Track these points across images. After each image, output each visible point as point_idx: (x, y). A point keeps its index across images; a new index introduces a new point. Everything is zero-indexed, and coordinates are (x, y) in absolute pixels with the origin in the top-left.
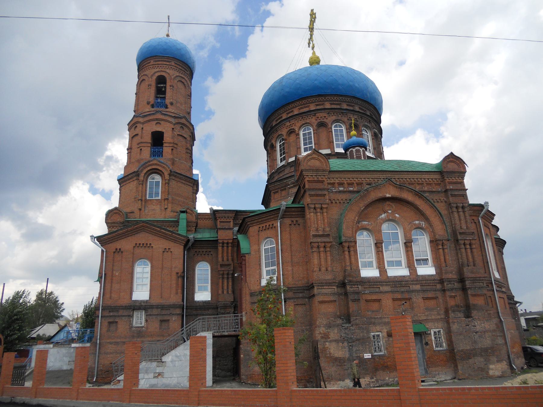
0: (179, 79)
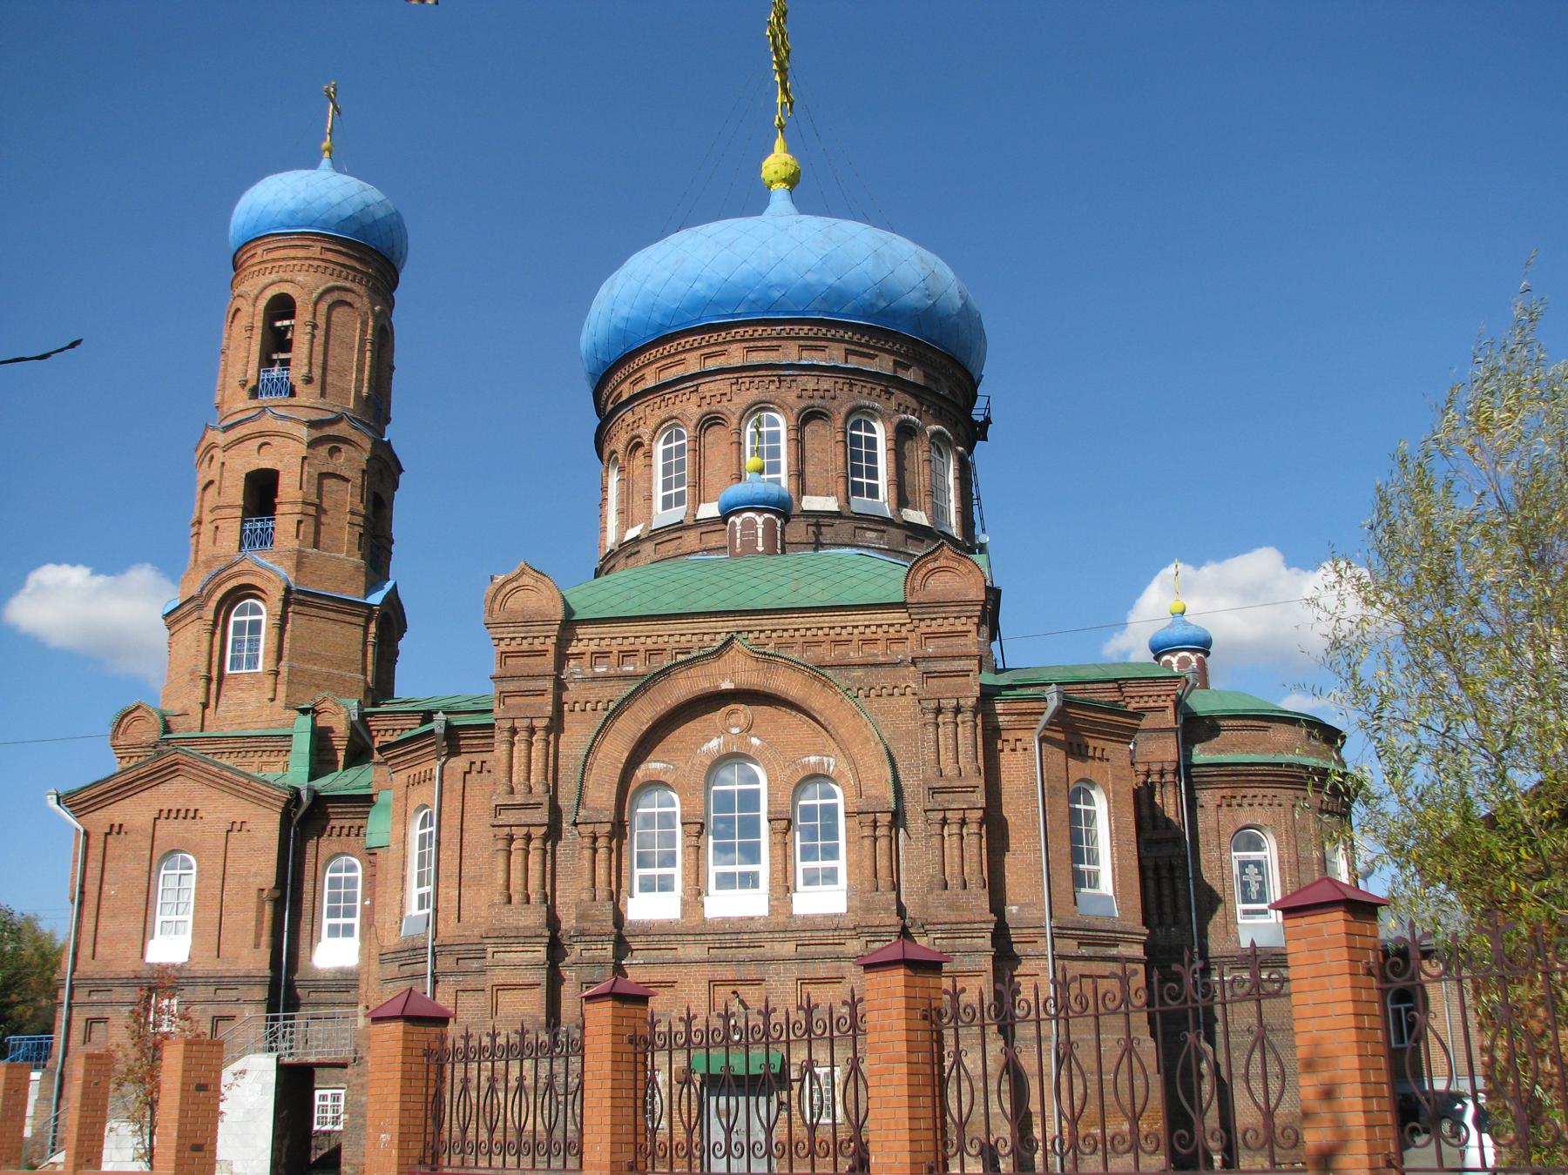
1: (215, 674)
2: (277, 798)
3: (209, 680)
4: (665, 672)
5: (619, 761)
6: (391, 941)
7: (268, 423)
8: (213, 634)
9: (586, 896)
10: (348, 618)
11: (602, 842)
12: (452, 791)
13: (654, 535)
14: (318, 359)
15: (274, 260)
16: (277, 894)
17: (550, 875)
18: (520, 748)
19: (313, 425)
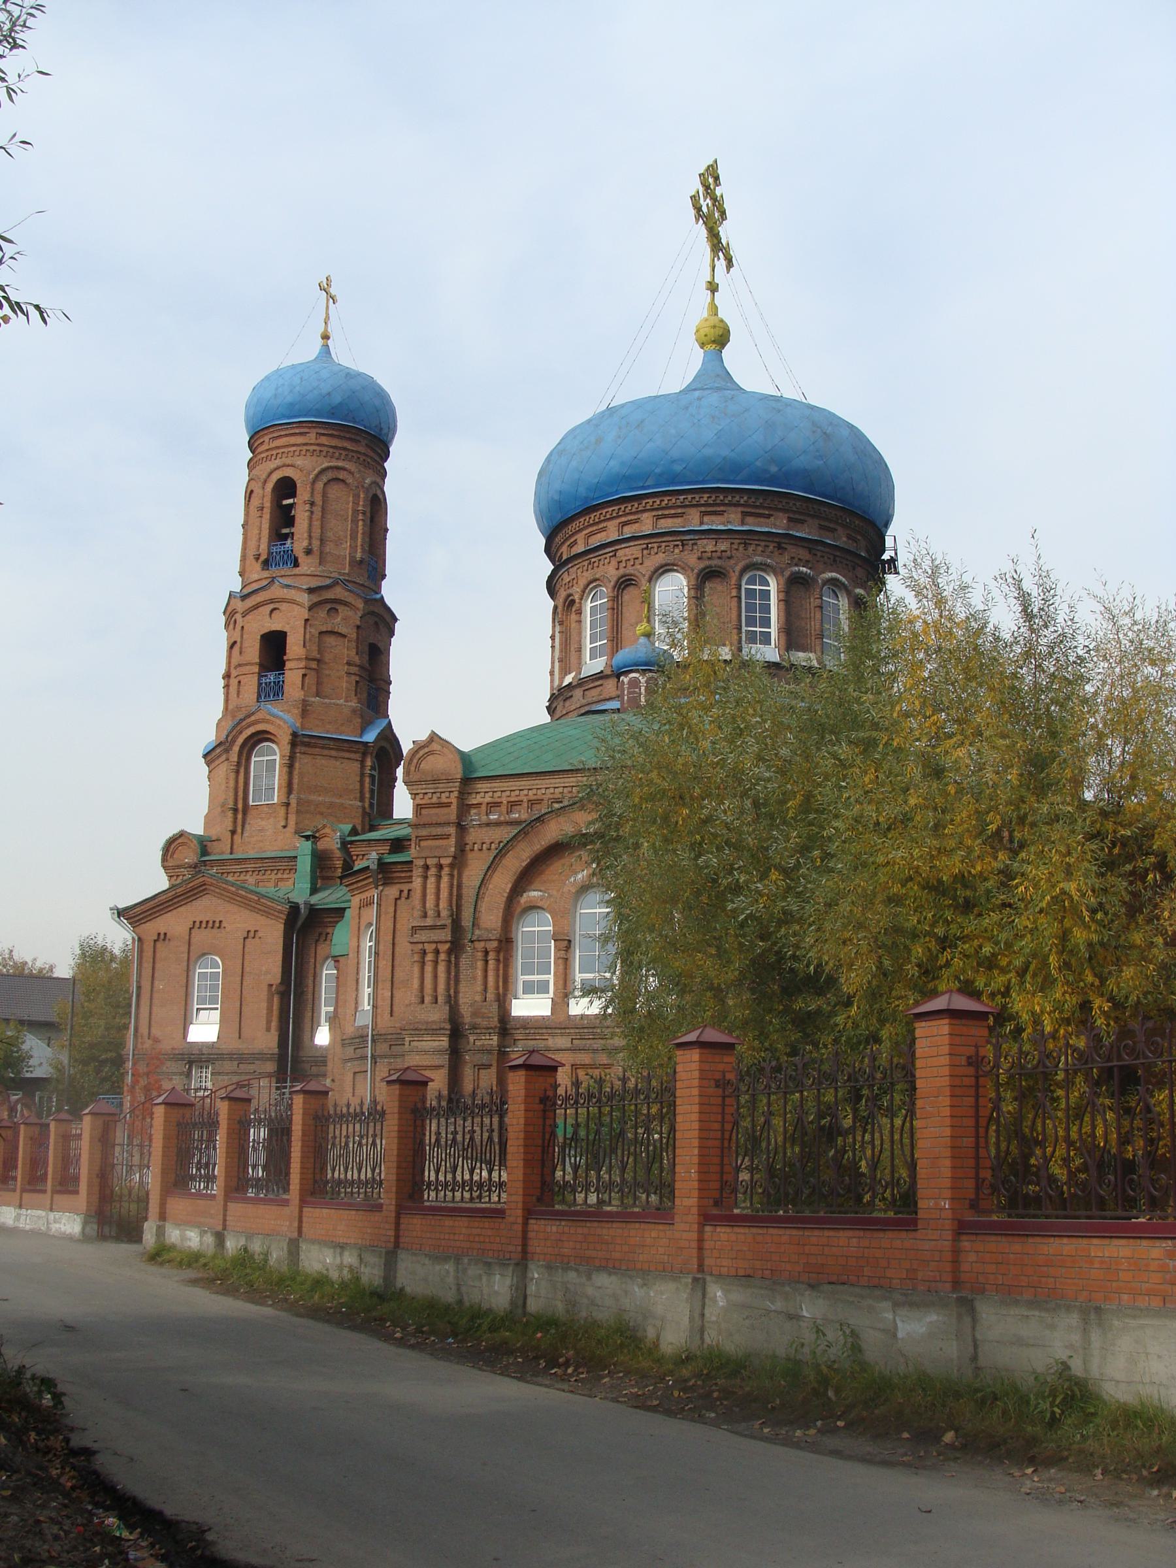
0: (330, 475)
1: (240, 806)
2: (280, 912)
3: (235, 810)
4: (540, 819)
5: (504, 891)
6: (350, 1030)
7: (276, 592)
8: (237, 772)
9: (478, 998)
10: (347, 755)
11: (492, 956)
12: (387, 913)
13: (581, 683)
14: (317, 532)
15: (278, 448)
16: (282, 988)
17: (454, 979)
18: (431, 881)
19: (311, 591)
